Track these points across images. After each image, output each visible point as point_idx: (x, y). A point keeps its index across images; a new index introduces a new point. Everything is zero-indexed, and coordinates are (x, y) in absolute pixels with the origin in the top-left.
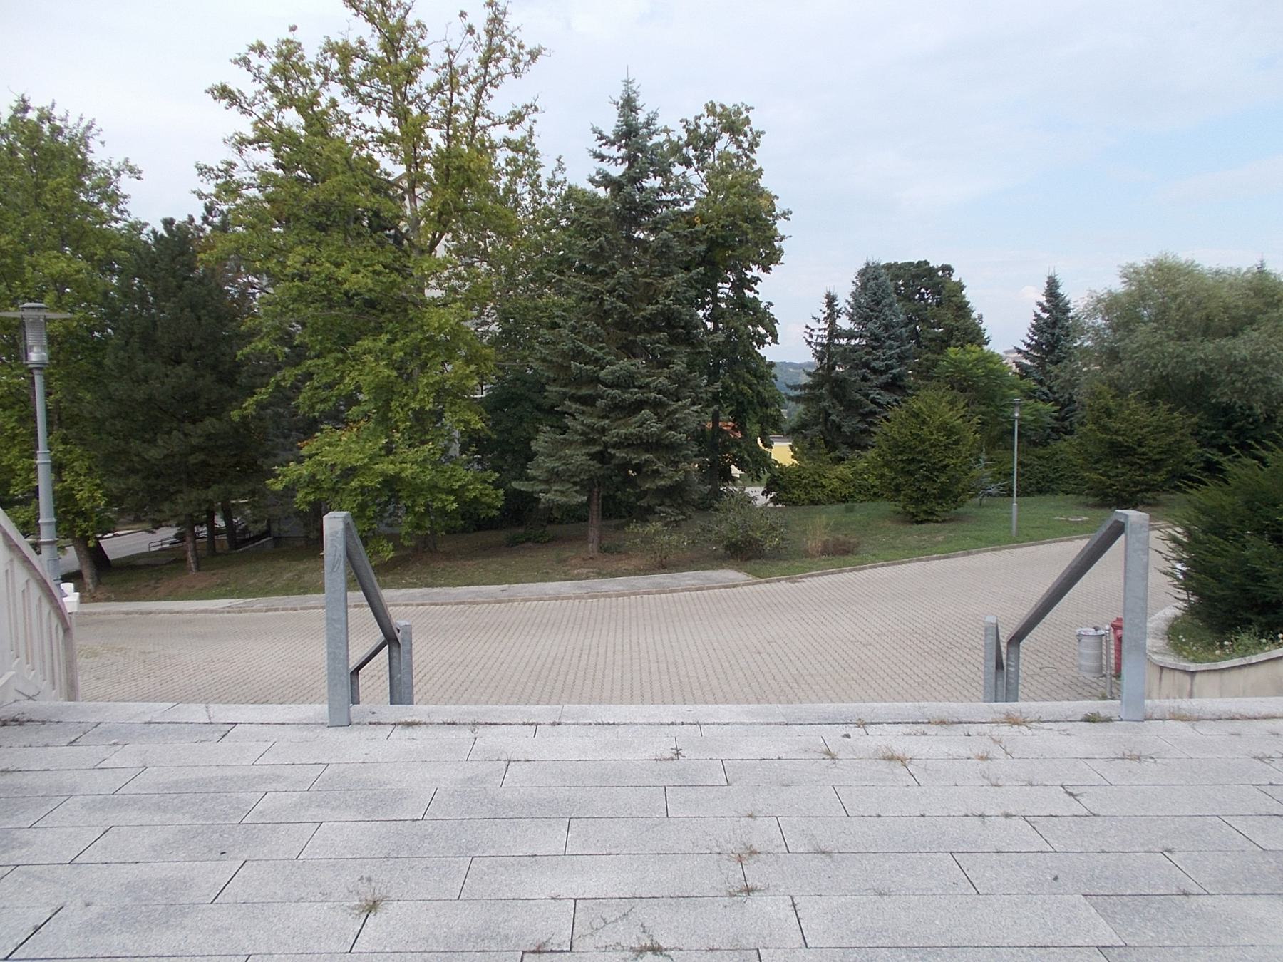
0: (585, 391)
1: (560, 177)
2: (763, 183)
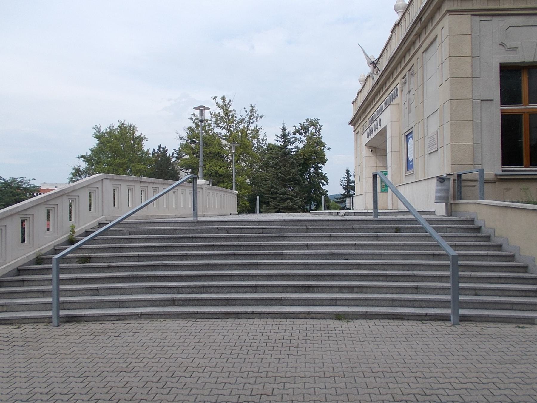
0: (274, 196)
1: (265, 138)
2: (323, 140)
